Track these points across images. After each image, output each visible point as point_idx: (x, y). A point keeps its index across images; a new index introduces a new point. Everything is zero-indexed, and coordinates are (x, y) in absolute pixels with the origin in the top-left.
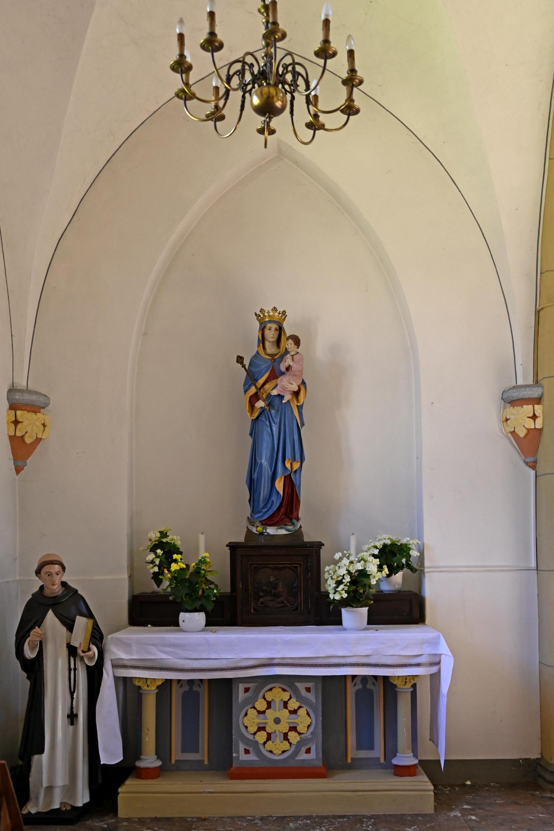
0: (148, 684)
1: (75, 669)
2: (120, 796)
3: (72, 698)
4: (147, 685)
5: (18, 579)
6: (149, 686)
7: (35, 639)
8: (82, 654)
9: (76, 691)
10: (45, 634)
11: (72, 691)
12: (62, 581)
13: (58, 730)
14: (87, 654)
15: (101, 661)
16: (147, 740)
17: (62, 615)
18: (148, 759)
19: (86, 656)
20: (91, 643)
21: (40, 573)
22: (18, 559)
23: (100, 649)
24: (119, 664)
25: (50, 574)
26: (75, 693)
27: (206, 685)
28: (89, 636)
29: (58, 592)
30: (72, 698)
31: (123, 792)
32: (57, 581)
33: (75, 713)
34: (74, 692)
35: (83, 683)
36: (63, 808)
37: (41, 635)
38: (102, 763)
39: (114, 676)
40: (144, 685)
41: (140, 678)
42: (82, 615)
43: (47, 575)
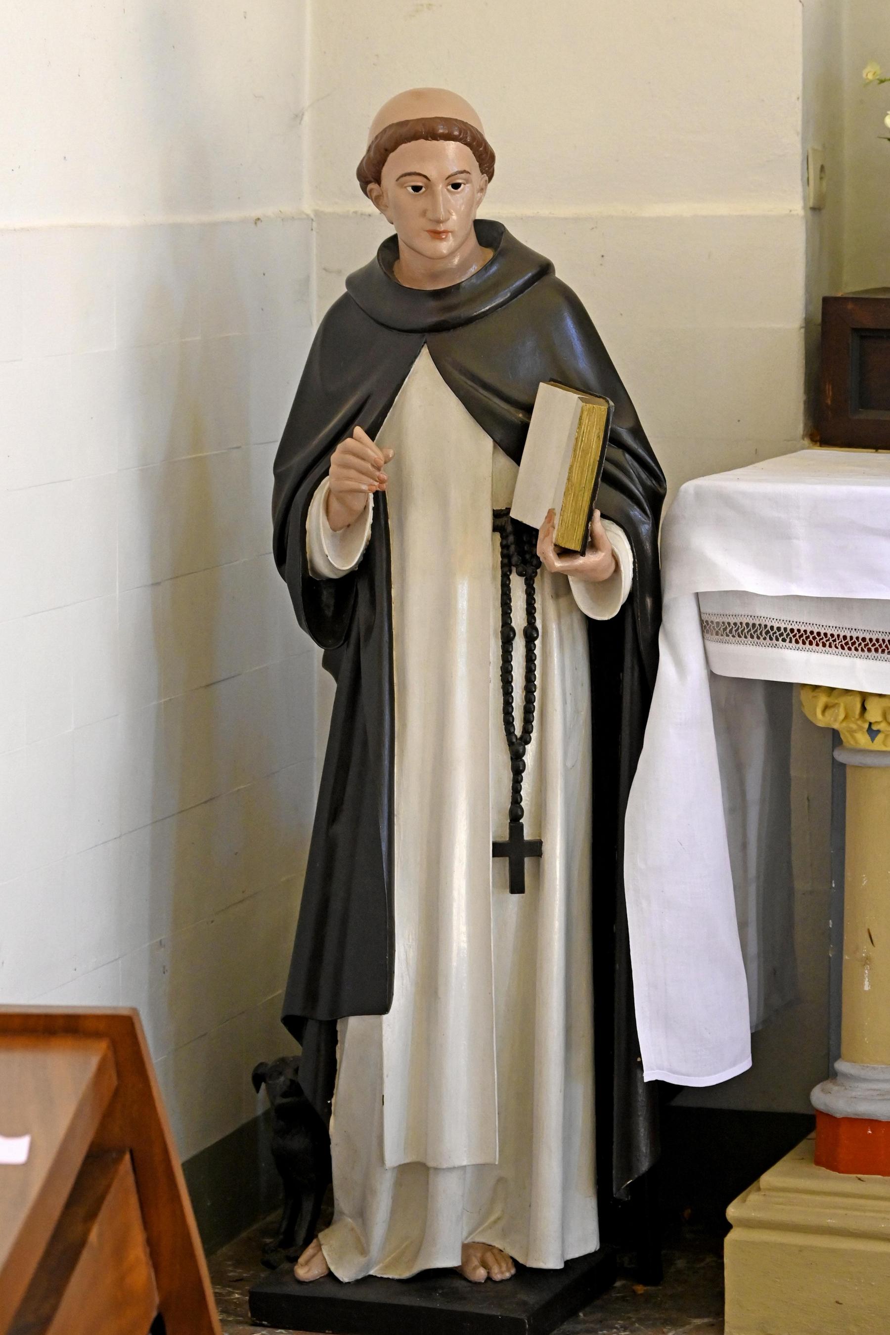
0: (872, 721)
1: (530, 635)
2: (730, 1239)
3: (518, 770)
4: (866, 726)
5: (308, 208)
6: (878, 731)
7: (352, 485)
8: (559, 564)
9: (534, 735)
10: (398, 461)
11: (518, 732)
12: (478, 218)
13: (455, 911)
14: (580, 561)
15: (649, 601)
16: (867, 987)
17: (474, 378)
18: (865, 1080)
19: (577, 571)
20: (597, 513)
21: (378, 181)
22: (307, 118)
23: (648, 546)
24: (732, 620)
25: (420, 184)
26: (528, 742)
27: (759, 697)
28: (588, 477)
29: (464, 266)
30: (518, 770)
31: (749, 1224)
32: (454, 217)
33: (528, 835)
34: (525, 739)
35: (569, 698)
36: (475, 1268)
37: (379, 469)
38: (649, 1076)
39: (713, 677)
40: (854, 726)
41: (833, 689)
42: (564, 380)
43: (410, 189)
